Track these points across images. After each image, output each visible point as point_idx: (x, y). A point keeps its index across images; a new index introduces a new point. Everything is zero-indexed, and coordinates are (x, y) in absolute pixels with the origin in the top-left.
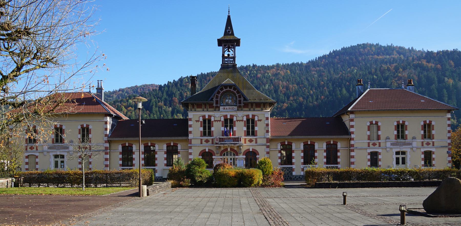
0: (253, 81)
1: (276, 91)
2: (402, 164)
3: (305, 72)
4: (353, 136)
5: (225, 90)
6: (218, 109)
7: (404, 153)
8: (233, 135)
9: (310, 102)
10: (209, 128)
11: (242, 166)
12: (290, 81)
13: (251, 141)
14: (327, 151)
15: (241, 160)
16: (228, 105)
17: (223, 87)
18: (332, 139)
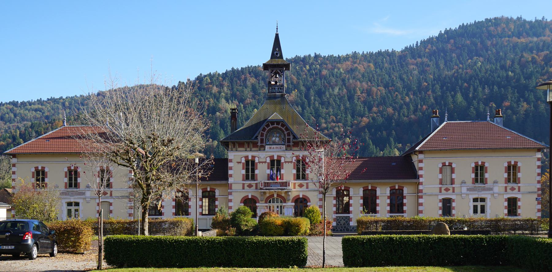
0: (314, 82)
1: (351, 98)
2: (481, 213)
3: (399, 66)
4: (421, 180)
5: (271, 127)
6: (263, 148)
7: (483, 200)
8: (280, 178)
9: (404, 115)
10: (253, 171)
11: (291, 214)
12: (374, 80)
13: (301, 186)
14: (365, 198)
15: (289, 209)
16: (274, 143)
17: (270, 123)
18: (397, 183)
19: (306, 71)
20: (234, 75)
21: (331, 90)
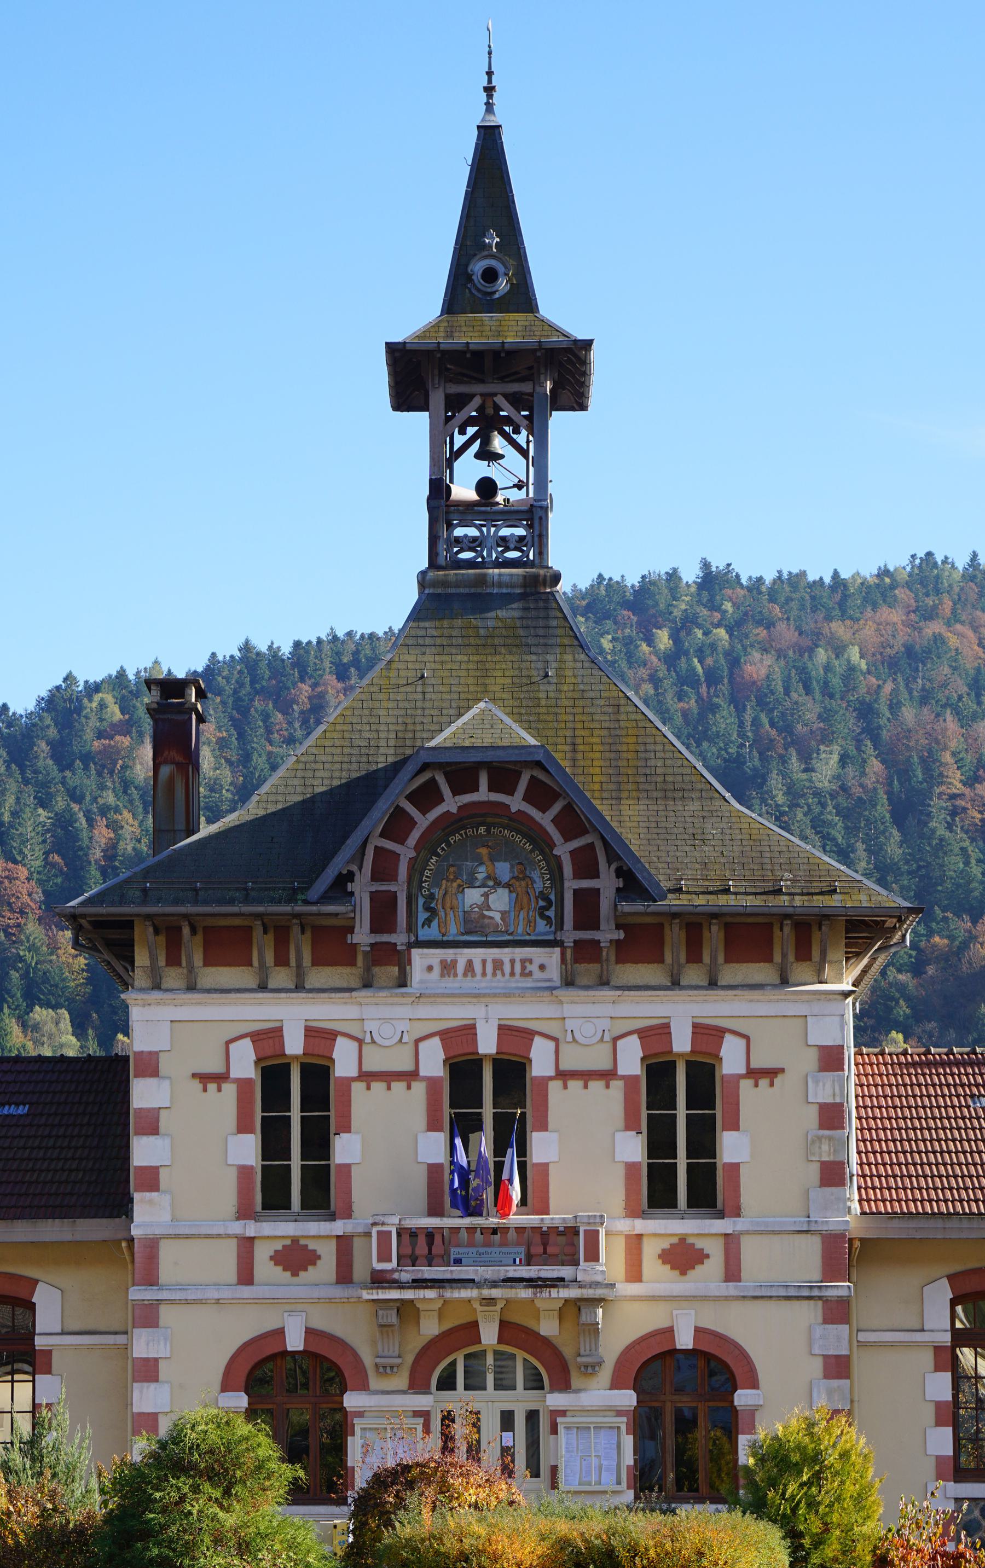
0: (702, 716)
5: (451, 803)
6: (395, 970)
8: (524, 1201)
11: (608, 1479)
19: (654, 659)
20: (252, 682)
21: (795, 763)
